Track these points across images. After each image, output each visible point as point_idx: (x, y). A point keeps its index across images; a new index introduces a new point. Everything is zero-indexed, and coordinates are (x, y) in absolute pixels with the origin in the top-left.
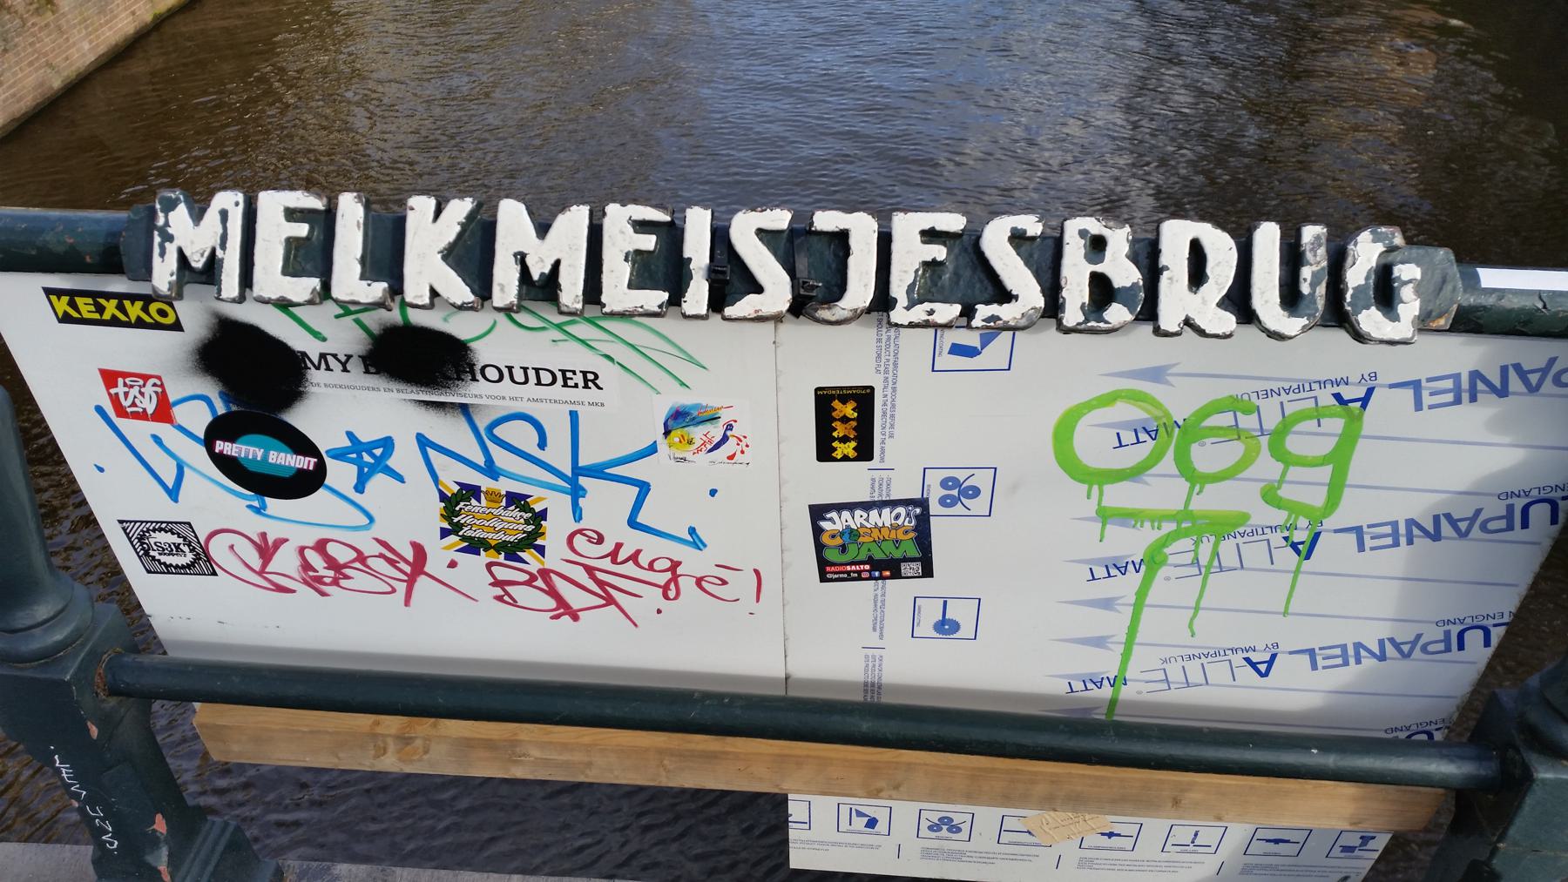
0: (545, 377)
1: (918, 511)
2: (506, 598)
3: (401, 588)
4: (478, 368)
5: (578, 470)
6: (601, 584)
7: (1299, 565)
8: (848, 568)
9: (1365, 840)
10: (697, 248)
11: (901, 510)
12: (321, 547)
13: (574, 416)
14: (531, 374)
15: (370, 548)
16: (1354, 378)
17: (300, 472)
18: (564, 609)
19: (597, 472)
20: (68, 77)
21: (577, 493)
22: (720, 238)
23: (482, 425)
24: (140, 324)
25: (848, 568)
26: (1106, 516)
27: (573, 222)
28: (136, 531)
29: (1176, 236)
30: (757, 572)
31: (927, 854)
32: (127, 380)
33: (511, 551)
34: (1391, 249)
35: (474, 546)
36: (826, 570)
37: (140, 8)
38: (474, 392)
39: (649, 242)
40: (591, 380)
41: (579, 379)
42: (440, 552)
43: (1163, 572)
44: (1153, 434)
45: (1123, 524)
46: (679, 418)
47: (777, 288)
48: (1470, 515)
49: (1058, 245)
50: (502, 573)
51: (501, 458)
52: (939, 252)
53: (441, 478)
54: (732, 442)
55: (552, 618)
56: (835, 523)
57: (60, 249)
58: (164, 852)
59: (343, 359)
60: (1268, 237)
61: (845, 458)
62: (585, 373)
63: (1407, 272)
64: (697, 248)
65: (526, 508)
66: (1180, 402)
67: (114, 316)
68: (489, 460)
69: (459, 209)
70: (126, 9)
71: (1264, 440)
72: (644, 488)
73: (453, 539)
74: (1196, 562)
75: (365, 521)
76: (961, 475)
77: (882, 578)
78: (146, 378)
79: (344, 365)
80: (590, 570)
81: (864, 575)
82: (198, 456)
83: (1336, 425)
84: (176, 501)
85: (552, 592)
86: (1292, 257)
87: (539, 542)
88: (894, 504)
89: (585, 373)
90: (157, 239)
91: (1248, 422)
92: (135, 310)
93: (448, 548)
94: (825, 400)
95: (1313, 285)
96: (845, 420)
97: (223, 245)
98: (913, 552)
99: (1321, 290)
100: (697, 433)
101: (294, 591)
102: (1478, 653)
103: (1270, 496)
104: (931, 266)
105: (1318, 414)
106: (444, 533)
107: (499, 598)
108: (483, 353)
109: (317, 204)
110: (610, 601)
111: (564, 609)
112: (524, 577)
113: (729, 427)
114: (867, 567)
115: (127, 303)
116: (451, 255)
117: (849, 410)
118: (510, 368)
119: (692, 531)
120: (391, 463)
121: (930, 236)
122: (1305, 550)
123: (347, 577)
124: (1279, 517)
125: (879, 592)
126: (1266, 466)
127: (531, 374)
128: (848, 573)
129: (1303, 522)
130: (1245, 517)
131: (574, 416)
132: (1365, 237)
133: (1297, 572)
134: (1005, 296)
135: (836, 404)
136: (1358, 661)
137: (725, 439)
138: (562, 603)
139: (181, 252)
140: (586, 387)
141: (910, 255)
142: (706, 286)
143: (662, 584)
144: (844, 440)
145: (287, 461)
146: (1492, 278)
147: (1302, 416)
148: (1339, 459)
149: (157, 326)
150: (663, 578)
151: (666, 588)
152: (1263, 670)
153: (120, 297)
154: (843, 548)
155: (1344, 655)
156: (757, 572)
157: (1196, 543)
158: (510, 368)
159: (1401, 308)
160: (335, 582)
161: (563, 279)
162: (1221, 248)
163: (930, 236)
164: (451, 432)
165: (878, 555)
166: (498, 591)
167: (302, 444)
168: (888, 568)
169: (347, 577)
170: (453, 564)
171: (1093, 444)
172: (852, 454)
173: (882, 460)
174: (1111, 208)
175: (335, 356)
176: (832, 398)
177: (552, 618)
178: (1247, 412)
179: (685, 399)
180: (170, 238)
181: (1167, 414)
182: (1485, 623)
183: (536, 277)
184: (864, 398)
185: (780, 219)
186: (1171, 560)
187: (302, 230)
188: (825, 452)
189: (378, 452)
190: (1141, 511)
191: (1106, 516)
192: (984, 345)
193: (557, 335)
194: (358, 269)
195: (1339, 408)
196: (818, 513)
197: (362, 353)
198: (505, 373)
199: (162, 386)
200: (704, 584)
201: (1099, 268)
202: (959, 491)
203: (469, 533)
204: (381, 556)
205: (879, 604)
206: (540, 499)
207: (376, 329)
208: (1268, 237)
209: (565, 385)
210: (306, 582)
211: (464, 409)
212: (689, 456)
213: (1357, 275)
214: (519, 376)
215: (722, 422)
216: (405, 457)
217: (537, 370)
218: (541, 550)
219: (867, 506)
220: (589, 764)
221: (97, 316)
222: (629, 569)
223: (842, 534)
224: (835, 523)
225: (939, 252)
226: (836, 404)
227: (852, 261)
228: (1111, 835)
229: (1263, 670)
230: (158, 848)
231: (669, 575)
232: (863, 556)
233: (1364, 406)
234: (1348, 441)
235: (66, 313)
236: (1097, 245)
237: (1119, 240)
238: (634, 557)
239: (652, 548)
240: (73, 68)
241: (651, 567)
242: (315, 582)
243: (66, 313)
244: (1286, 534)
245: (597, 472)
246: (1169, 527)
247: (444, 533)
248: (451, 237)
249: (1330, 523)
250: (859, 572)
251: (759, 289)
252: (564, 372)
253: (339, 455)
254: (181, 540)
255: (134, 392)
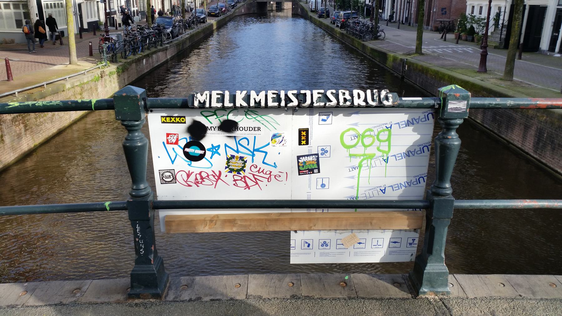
0: (251, 129)
1: (317, 156)
2: (236, 184)
3: (215, 183)
4: (239, 128)
5: (254, 150)
6: (255, 179)
7: (386, 165)
8: (304, 171)
9: (414, 240)
10: (283, 96)
11: (314, 156)
12: (200, 174)
13: (255, 137)
14: (248, 128)
15: (210, 173)
16: (388, 123)
17: (201, 154)
18: (248, 187)
19: (258, 150)
20: (5, 164)
21: (253, 155)
22: (286, 95)
23: (237, 141)
24: (178, 123)
25: (304, 171)
26: (351, 156)
27: (263, 94)
28: (162, 173)
29: (355, 92)
30: (286, 173)
31: (322, 255)
32: (171, 135)
33: (238, 171)
34: (387, 93)
35: (231, 171)
36: (300, 172)
37: (30, 143)
38: (237, 133)
39: (275, 96)
40: (259, 129)
41: (257, 129)
42: (225, 172)
43: (362, 168)
44: (357, 137)
45: (354, 158)
46: (274, 136)
47: (295, 102)
48: (414, 150)
49: (338, 95)
50: (236, 178)
51: (241, 148)
52: (320, 95)
53: (228, 154)
54: (284, 141)
55: (245, 189)
56: (302, 160)
57: (174, 103)
58: (152, 255)
59: (214, 127)
60: (369, 92)
61: (304, 145)
62: (258, 128)
63: (390, 95)
64: (283, 96)
65: (243, 160)
66: (361, 130)
67: (173, 121)
68: (238, 149)
69: (244, 92)
70: (26, 143)
71: (376, 137)
72: (266, 153)
73: (228, 169)
74: (368, 166)
75: (210, 165)
76: (324, 147)
77: (310, 174)
78: (175, 134)
79: (214, 129)
80: (254, 175)
81: (307, 173)
82: (181, 152)
83: (387, 133)
84: (173, 164)
85: (245, 182)
86: (373, 95)
87: (244, 169)
88: (312, 155)
89: (258, 128)
90: (195, 98)
91: (372, 133)
92: (177, 119)
93: (226, 172)
94: (300, 131)
95: (376, 98)
96: (304, 136)
97: (206, 99)
98: (316, 167)
99: (377, 98)
100: (277, 139)
101: (192, 186)
102: (423, 184)
103: (379, 150)
104: (319, 97)
105: (384, 131)
106: (226, 168)
107: (234, 185)
108: (240, 125)
109: (222, 92)
110: (257, 183)
111: (248, 187)
112: (240, 178)
113: (283, 138)
114: (308, 171)
115: (176, 118)
116: (244, 99)
117: (304, 133)
118: (245, 127)
119: (275, 163)
120: (219, 151)
121: (319, 93)
122: (386, 161)
123: (204, 181)
124: (381, 154)
125: (310, 177)
126: (377, 143)
127: (248, 128)
128: (304, 173)
129: (385, 155)
130: (375, 154)
131: (255, 137)
132: (383, 91)
133: (386, 166)
134: (331, 101)
135: (302, 132)
136: (401, 188)
137: (282, 140)
138: (247, 185)
139: (199, 100)
140: (258, 131)
141: (316, 96)
142: (284, 102)
143: (268, 178)
144: (304, 140)
145: (199, 152)
146: (404, 99)
147: (381, 132)
148: (389, 140)
149: (181, 123)
150: (267, 176)
151: (268, 179)
152: (384, 192)
153: (175, 117)
154: (303, 166)
155: (398, 187)
156: (286, 173)
157: (367, 161)
158: (245, 127)
159: (389, 100)
160: (201, 183)
161: (261, 101)
162: (362, 94)
163: (319, 93)
164: (232, 143)
165: (310, 168)
166: (234, 183)
167: (202, 148)
168: (311, 171)
169: (204, 181)
170: (226, 176)
171: (348, 141)
172: (305, 143)
173: (310, 145)
174: (345, 89)
175: (213, 127)
176: (301, 131)
177: (245, 189)
178: (372, 131)
179: (275, 132)
180: (197, 98)
181: (359, 133)
182: (422, 176)
183: (257, 101)
184: (307, 131)
185: (295, 92)
186: (363, 165)
187: (219, 96)
188: (300, 144)
189: (217, 148)
190: (357, 154)
191: (351, 156)
192: (327, 119)
193: (254, 120)
194: (228, 102)
195: (387, 129)
196: (299, 158)
197: (218, 126)
198: (244, 129)
199: (178, 136)
200: (276, 177)
201: (345, 97)
202: (325, 151)
203: (231, 168)
204: (212, 175)
205: (310, 180)
206: (246, 158)
207: (222, 121)
208: (369, 92)
209: (254, 130)
210: (195, 184)
211: (235, 137)
212: (275, 145)
213: (382, 96)
214: (246, 129)
215: (282, 137)
216: (222, 150)
217: (249, 127)
218: (244, 171)
219: (308, 156)
220: (250, 225)
221: (170, 121)
222: (261, 174)
223: (303, 163)
224: (302, 160)
225: (320, 95)
226: (302, 132)
227: (307, 97)
228: (360, 243)
229: (384, 192)
230: (151, 254)
231: (269, 175)
232: (307, 169)
233: (391, 128)
234: (390, 135)
235: (164, 121)
236: (344, 94)
237: (347, 93)
238: (263, 171)
239: (267, 168)
240: (7, 161)
241: (266, 174)
242: (197, 183)
243: (164, 121)
244: (383, 158)
245: (258, 150)
246: (362, 158)
247: (226, 168)
248: (243, 96)
249: (390, 154)
250: (306, 172)
251: (293, 102)
252: (254, 127)
253: (209, 150)
254: (171, 174)
255: (172, 138)
